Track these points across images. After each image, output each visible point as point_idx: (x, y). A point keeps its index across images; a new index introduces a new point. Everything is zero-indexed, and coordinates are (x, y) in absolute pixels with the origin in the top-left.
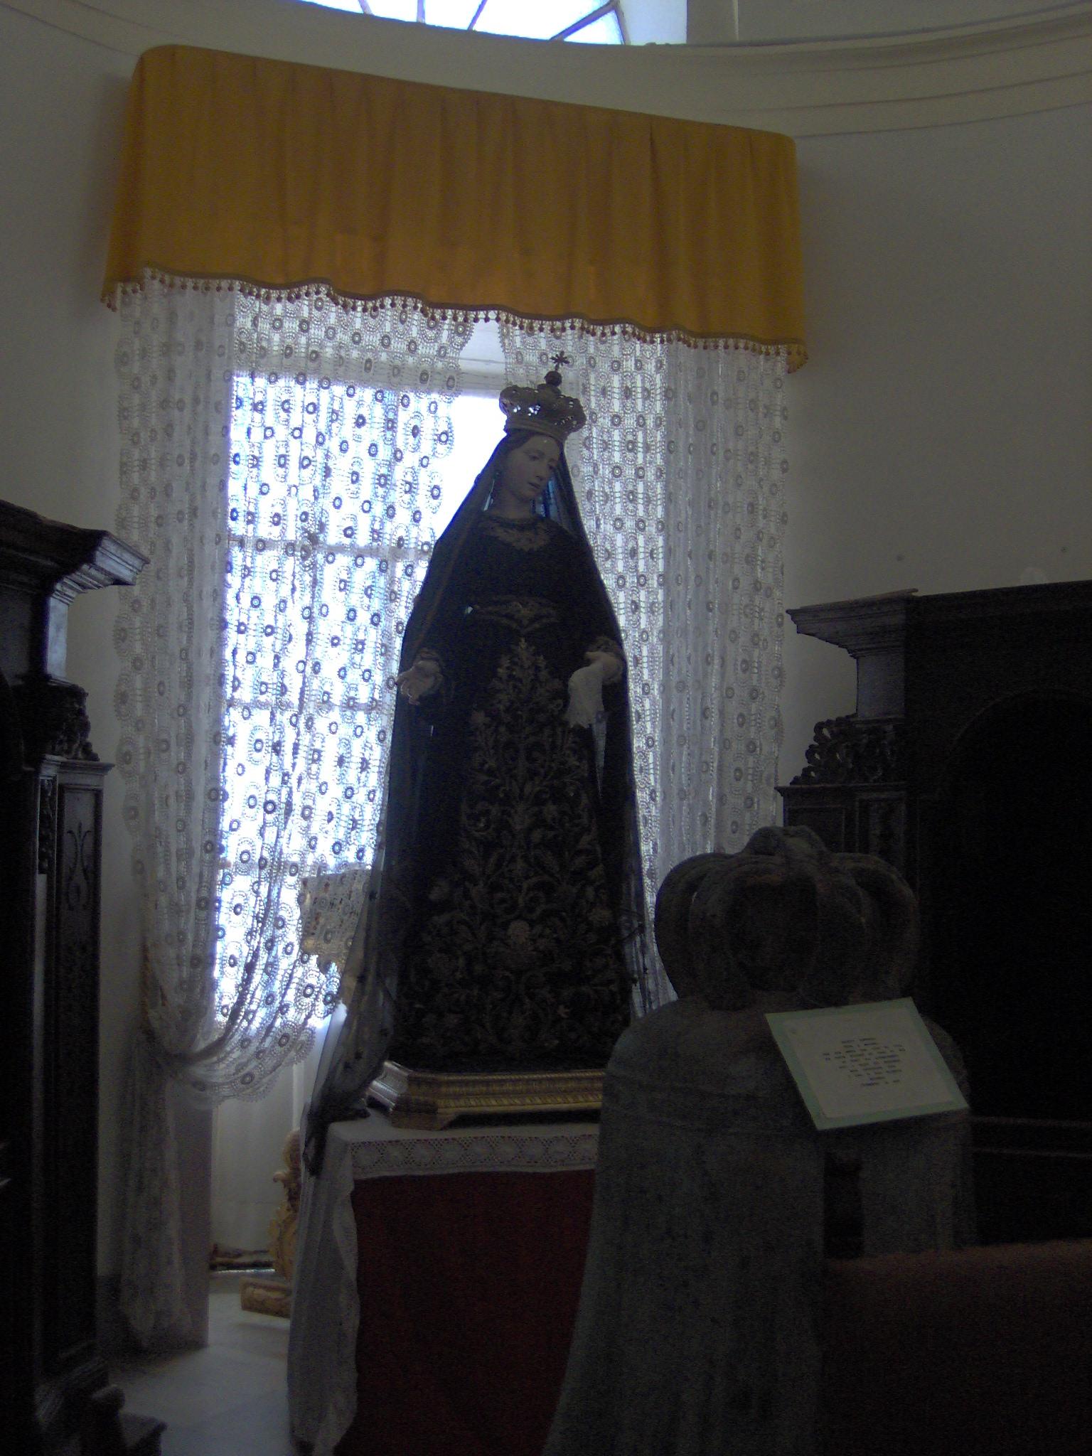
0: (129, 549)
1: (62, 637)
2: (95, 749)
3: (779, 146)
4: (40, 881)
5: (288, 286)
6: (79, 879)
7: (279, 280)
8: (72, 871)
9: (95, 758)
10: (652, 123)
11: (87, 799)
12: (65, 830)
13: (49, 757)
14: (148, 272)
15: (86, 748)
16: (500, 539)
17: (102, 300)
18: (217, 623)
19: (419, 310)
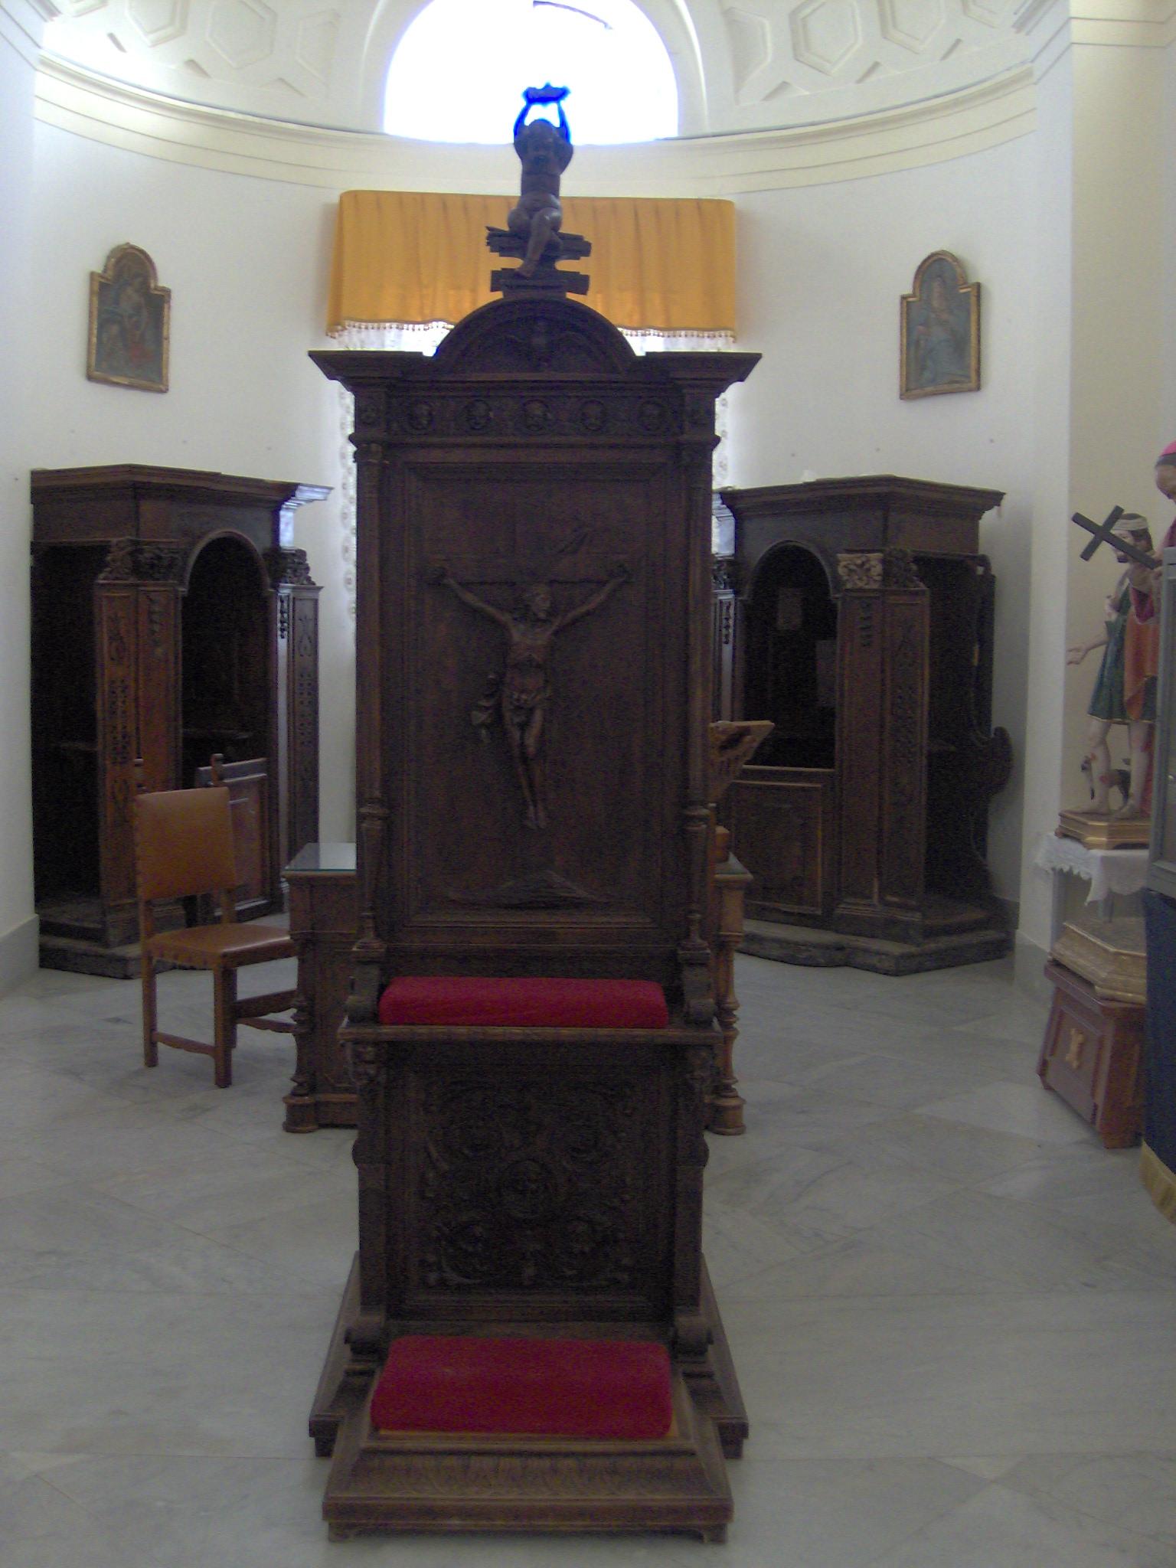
0: (291, 706)
1: (290, 528)
2: (313, 580)
3: (720, 206)
4: (282, 644)
5: (425, 322)
6: (306, 642)
7: (419, 320)
8: (302, 638)
9: (314, 584)
10: (699, 203)
11: (309, 605)
12: (296, 618)
13: (282, 584)
14: (347, 323)
15: (309, 579)
16: (822, 646)
17: (327, 335)
18: (385, 433)
19: (1126, 617)
